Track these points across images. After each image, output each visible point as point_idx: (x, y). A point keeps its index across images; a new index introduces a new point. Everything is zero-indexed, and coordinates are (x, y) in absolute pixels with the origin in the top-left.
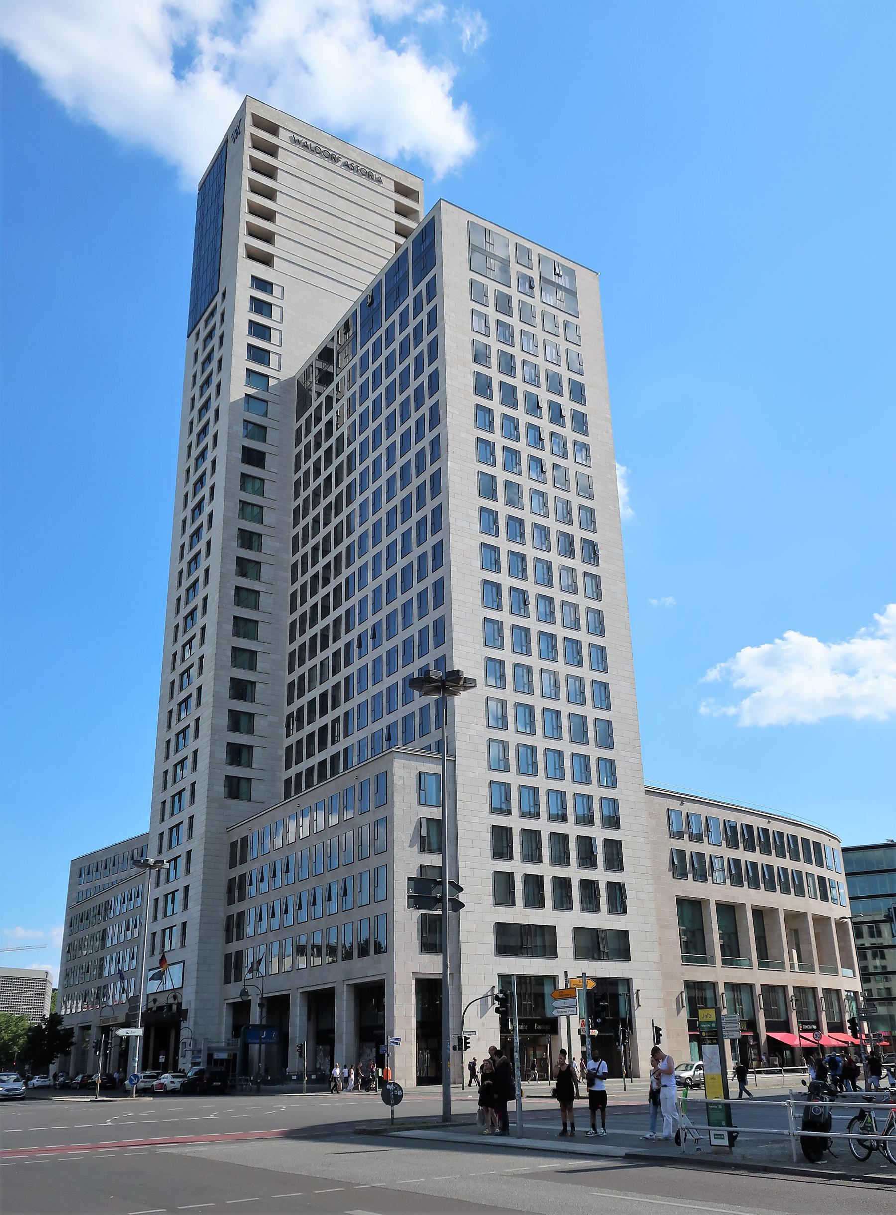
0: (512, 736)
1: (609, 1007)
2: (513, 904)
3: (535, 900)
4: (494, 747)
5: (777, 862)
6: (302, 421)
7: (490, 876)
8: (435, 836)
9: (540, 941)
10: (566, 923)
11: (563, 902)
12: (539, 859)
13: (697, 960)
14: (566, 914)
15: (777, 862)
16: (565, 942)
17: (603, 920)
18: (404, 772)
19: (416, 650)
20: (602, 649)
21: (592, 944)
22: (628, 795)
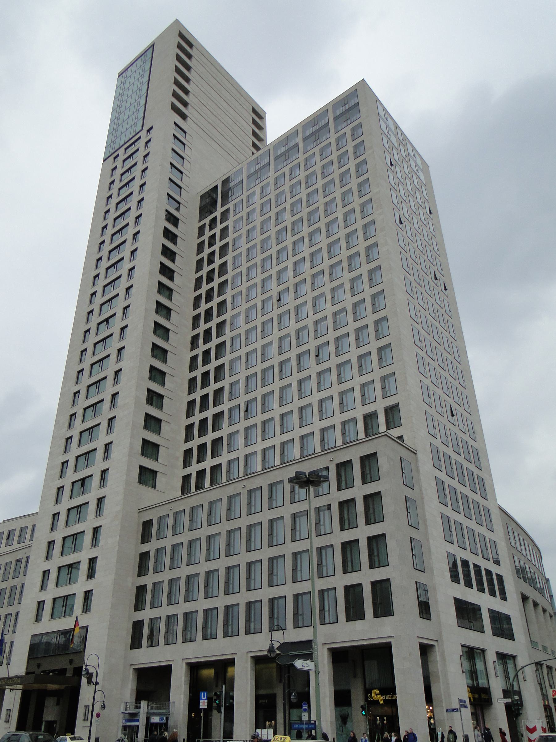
6: (207, 221)
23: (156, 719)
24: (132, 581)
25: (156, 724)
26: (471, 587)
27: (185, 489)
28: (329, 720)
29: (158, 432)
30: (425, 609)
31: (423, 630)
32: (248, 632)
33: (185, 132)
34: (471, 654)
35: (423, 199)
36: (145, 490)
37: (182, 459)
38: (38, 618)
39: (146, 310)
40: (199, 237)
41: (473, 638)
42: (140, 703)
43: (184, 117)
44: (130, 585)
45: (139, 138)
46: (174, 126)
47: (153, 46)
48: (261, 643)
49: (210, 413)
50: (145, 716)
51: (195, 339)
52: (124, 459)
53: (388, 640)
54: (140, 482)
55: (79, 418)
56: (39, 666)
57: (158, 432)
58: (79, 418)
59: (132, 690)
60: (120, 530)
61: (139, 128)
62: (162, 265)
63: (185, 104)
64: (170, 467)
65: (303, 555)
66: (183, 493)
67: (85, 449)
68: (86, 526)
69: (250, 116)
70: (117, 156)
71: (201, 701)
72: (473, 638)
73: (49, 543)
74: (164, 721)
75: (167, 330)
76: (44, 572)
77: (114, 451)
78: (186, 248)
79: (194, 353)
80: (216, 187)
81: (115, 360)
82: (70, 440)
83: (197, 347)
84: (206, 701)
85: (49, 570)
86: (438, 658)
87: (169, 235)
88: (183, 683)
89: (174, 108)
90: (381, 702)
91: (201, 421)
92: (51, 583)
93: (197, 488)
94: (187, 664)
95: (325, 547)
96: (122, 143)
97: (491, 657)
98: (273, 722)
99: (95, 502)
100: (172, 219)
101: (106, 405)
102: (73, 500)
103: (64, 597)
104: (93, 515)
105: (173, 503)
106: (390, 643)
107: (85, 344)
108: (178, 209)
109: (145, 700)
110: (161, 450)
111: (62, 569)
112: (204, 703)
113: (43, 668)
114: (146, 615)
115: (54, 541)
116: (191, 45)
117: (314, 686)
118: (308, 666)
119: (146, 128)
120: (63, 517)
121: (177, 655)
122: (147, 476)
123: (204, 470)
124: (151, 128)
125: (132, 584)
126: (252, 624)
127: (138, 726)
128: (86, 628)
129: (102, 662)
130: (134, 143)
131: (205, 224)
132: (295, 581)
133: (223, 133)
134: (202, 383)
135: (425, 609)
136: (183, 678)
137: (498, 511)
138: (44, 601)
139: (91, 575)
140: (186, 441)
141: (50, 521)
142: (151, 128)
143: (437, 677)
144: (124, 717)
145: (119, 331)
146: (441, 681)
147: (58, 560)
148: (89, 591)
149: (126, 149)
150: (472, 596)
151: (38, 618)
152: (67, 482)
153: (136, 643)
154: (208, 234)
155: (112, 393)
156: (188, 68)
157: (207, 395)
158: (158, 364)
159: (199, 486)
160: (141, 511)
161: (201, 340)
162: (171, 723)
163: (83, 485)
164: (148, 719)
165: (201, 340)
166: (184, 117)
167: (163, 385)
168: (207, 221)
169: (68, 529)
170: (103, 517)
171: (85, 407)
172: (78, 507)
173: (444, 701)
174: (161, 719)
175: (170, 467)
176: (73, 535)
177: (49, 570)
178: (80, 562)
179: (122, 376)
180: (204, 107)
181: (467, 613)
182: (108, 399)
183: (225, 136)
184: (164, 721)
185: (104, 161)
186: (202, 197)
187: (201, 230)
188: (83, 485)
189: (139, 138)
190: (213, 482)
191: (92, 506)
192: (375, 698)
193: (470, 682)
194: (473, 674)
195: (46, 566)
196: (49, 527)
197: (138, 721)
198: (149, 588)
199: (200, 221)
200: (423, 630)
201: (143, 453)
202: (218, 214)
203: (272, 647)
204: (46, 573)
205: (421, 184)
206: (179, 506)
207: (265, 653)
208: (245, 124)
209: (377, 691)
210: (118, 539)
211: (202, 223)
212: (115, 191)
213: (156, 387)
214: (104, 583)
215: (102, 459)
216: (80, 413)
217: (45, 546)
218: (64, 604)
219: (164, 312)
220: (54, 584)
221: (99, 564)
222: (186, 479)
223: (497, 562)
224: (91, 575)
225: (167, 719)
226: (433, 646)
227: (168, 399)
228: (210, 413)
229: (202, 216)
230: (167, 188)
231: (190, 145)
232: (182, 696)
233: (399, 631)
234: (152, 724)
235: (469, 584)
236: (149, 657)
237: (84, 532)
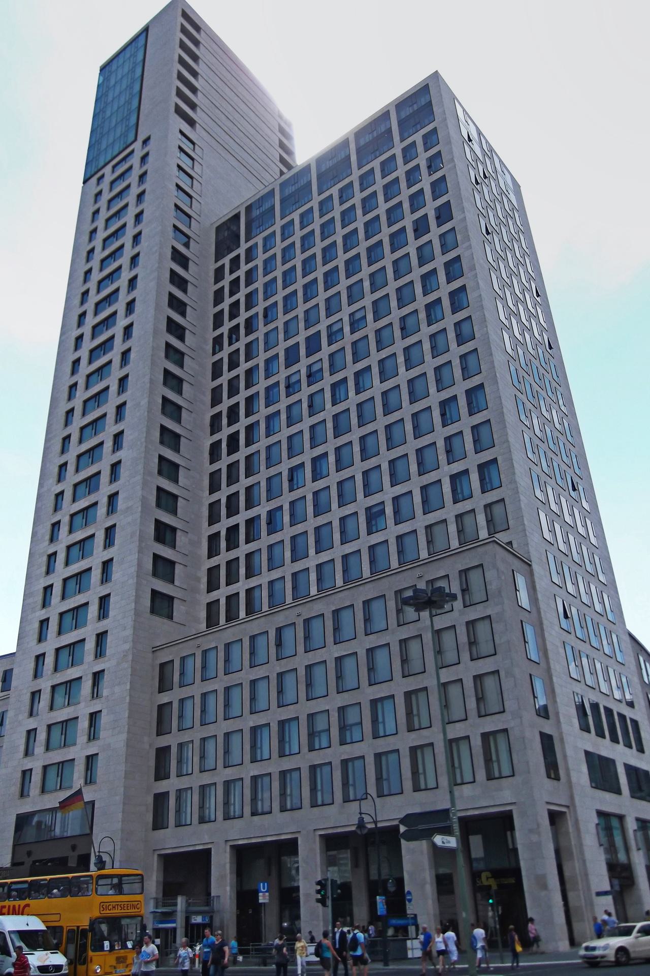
6: (226, 261)
23: (198, 919)
24: (151, 742)
25: (198, 925)
26: (603, 737)
27: (212, 620)
28: (431, 911)
30: (552, 769)
31: (545, 793)
32: (314, 805)
33: (193, 143)
34: (609, 822)
35: (484, 205)
36: (159, 622)
37: (204, 580)
39: (152, 382)
40: (216, 283)
41: (609, 802)
42: (176, 899)
43: (191, 123)
45: (133, 151)
46: (180, 136)
47: (146, 30)
48: (341, 817)
49: (241, 519)
50: (184, 915)
51: (216, 418)
53: (508, 808)
54: (153, 611)
55: (64, 529)
58: (64, 529)
59: (157, 882)
61: (131, 137)
62: (170, 321)
63: (193, 106)
65: (386, 702)
66: (209, 626)
70: (103, 176)
71: (260, 894)
72: (609, 802)
73: (33, 694)
74: (207, 920)
75: (179, 408)
76: (29, 732)
77: (117, 573)
78: (199, 297)
79: (216, 437)
80: (237, 217)
81: (111, 449)
82: (53, 558)
83: (220, 429)
84: (267, 894)
85: (36, 729)
86: (571, 830)
87: (178, 281)
88: (228, 871)
89: (179, 111)
90: (494, 887)
91: (229, 530)
92: (39, 748)
93: (228, 619)
94: (232, 847)
95: (416, 692)
96: (109, 158)
97: (631, 825)
98: (348, 919)
99: (94, 638)
100: (180, 258)
101: (102, 510)
102: (62, 637)
103: (59, 763)
104: (92, 657)
105: (200, 639)
106: (511, 811)
107: (69, 428)
108: (187, 245)
109: (182, 894)
110: (178, 569)
111: (53, 727)
112: (264, 896)
113: (34, 857)
114: (171, 785)
115: (40, 691)
116: (198, 28)
118: (449, 842)
119: (141, 137)
120: (49, 660)
121: (219, 838)
122: (161, 604)
124: (148, 139)
125: (150, 745)
126: (319, 794)
127: (175, 929)
128: (92, 803)
129: (118, 847)
130: (124, 159)
131: (223, 265)
132: (376, 736)
133: (242, 144)
134: (229, 477)
135: (552, 769)
136: (228, 866)
137: (627, 638)
138: (31, 770)
139: (93, 736)
140: (210, 556)
141: (32, 665)
142: (148, 139)
143: (571, 854)
144: (154, 918)
145: (114, 410)
146: (575, 858)
147: (45, 717)
148: (92, 756)
149: (114, 167)
150: (605, 748)
151: (23, 794)
153: (159, 823)
154: (228, 278)
155: (109, 493)
156: (195, 58)
158: (169, 454)
159: (231, 616)
160: (155, 650)
161: (225, 421)
162: (217, 922)
164: (187, 919)
165: (225, 421)
166: (191, 123)
167: (176, 481)
168: (226, 261)
169: (58, 675)
170: (106, 659)
171: (72, 512)
172: (69, 645)
173: (580, 882)
174: (203, 919)
176: (66, 682)
177: (36, 729)
178: (77, 718)
179: (122, 470)
180: (217, 111)
181: (602, 772)
183: (245, 148)
184: (207, 920)
185: (84, 183)
186: (219, 229)
187: (219, 274)
189: (133, 151)
190: (250, 611)
191: (90, 645)
192: (485, 883)
193: (609, 857)
194: (611, 849)
195: (31, 724)
196: (31, 673)
197: (174, 922)
198: (174, 750)
199: (216, 261)
200: (545, 793)
202: (241, 251)
203: (361, 820)
204: (31, 734)
205: (513, 209)
206: (209, 643)
207: (353, 828)
209: (489, 874)
210: (128, 687)
211: (220, 263)
212: (100, 223)
215: (99, 582)
216: (66, 520)
217: (27, 698)
219: (174, 382)
220: (43, 748)
222: (212, 607)
223: (631, 704)
224: (93, 736)
225: (211, 918)
226: (563, 813)
227: (184, 501)
228: (241, 519)
229: (219, 256)
230: (171, 218)
231: (200, 160)
232: (228, 888)
233: (526, 796)
234: (193, 925)
235: (600, 734)
236: (178, 840)
237: (81, 678)
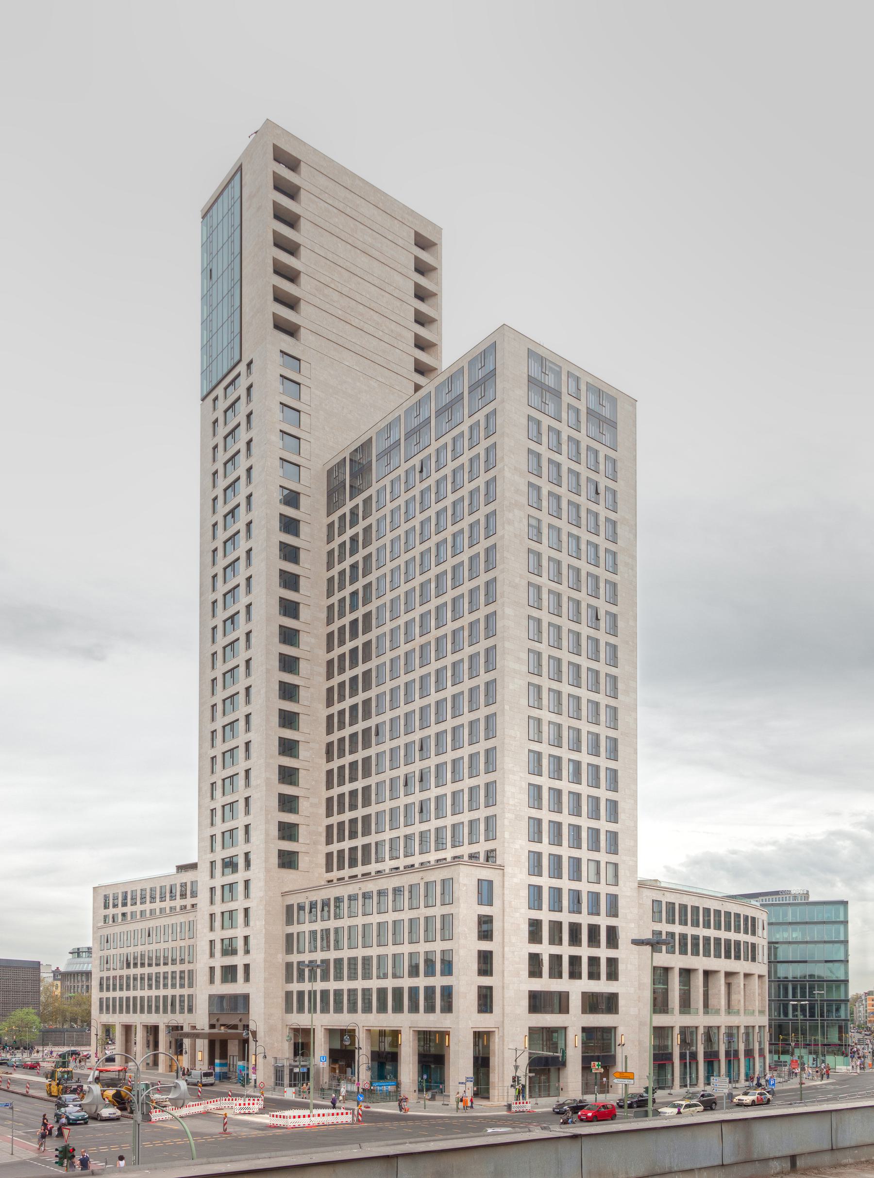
0: (545, 848)
1: (600, 1047)
2: (560, 977)
3: (556, 973)
4: (655, 904)
5: (702, 932)
6: (335, 517)
7: (527, 957)
8: (485, 928)
9: (560, 1002)
10: (577, 989)
11: (575, 974)
12: (540, 942)
13: (342, 1032)
14: (577, 982)
15: (702, 932)
16: (575, 1002)
17: (602, 986)
18: (466, 879)
19: (466, 771)
20: (615, 772)
21: (596, 1003)
22: (625, 891)
29: (296, 534)
38: (212, 981)
39: (268, 671)
44: (280, 961)
47: (240, 168)
52: (263, 844)
56: (218, 1020)
57: (296, 534)
60: (266, 980)
64: (312, 847)
67: (230, 558)
68: (240, 795)
69: (406, 256)
117: (579, 1043)
122: (288, 860)
123: (357, 676)
152: (218, 622)
157: (356, 620)
163: (233, 623)
175: (312, 847)
182: (243, 557)
188: (233, 623)
201: (282, 837)
208: (398, 278)
213: (290, 567)
214: (258, 929)
218: (229, 973)
221: (252, 857)
